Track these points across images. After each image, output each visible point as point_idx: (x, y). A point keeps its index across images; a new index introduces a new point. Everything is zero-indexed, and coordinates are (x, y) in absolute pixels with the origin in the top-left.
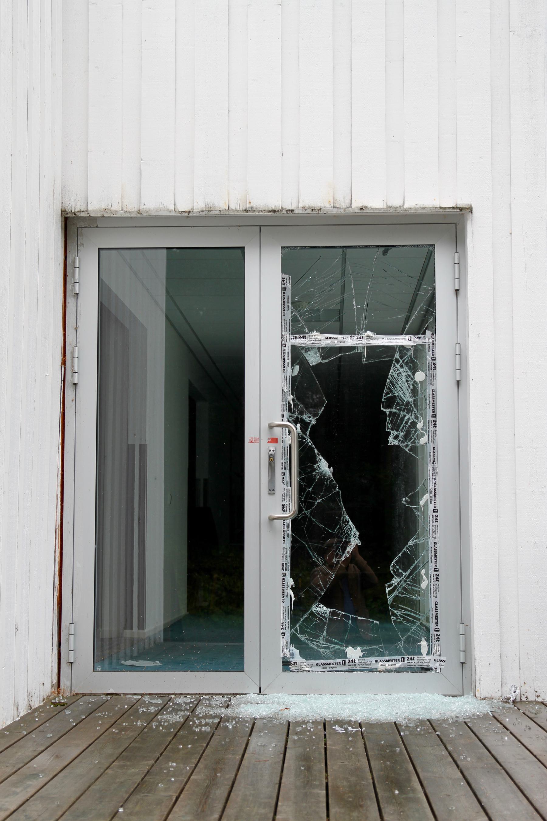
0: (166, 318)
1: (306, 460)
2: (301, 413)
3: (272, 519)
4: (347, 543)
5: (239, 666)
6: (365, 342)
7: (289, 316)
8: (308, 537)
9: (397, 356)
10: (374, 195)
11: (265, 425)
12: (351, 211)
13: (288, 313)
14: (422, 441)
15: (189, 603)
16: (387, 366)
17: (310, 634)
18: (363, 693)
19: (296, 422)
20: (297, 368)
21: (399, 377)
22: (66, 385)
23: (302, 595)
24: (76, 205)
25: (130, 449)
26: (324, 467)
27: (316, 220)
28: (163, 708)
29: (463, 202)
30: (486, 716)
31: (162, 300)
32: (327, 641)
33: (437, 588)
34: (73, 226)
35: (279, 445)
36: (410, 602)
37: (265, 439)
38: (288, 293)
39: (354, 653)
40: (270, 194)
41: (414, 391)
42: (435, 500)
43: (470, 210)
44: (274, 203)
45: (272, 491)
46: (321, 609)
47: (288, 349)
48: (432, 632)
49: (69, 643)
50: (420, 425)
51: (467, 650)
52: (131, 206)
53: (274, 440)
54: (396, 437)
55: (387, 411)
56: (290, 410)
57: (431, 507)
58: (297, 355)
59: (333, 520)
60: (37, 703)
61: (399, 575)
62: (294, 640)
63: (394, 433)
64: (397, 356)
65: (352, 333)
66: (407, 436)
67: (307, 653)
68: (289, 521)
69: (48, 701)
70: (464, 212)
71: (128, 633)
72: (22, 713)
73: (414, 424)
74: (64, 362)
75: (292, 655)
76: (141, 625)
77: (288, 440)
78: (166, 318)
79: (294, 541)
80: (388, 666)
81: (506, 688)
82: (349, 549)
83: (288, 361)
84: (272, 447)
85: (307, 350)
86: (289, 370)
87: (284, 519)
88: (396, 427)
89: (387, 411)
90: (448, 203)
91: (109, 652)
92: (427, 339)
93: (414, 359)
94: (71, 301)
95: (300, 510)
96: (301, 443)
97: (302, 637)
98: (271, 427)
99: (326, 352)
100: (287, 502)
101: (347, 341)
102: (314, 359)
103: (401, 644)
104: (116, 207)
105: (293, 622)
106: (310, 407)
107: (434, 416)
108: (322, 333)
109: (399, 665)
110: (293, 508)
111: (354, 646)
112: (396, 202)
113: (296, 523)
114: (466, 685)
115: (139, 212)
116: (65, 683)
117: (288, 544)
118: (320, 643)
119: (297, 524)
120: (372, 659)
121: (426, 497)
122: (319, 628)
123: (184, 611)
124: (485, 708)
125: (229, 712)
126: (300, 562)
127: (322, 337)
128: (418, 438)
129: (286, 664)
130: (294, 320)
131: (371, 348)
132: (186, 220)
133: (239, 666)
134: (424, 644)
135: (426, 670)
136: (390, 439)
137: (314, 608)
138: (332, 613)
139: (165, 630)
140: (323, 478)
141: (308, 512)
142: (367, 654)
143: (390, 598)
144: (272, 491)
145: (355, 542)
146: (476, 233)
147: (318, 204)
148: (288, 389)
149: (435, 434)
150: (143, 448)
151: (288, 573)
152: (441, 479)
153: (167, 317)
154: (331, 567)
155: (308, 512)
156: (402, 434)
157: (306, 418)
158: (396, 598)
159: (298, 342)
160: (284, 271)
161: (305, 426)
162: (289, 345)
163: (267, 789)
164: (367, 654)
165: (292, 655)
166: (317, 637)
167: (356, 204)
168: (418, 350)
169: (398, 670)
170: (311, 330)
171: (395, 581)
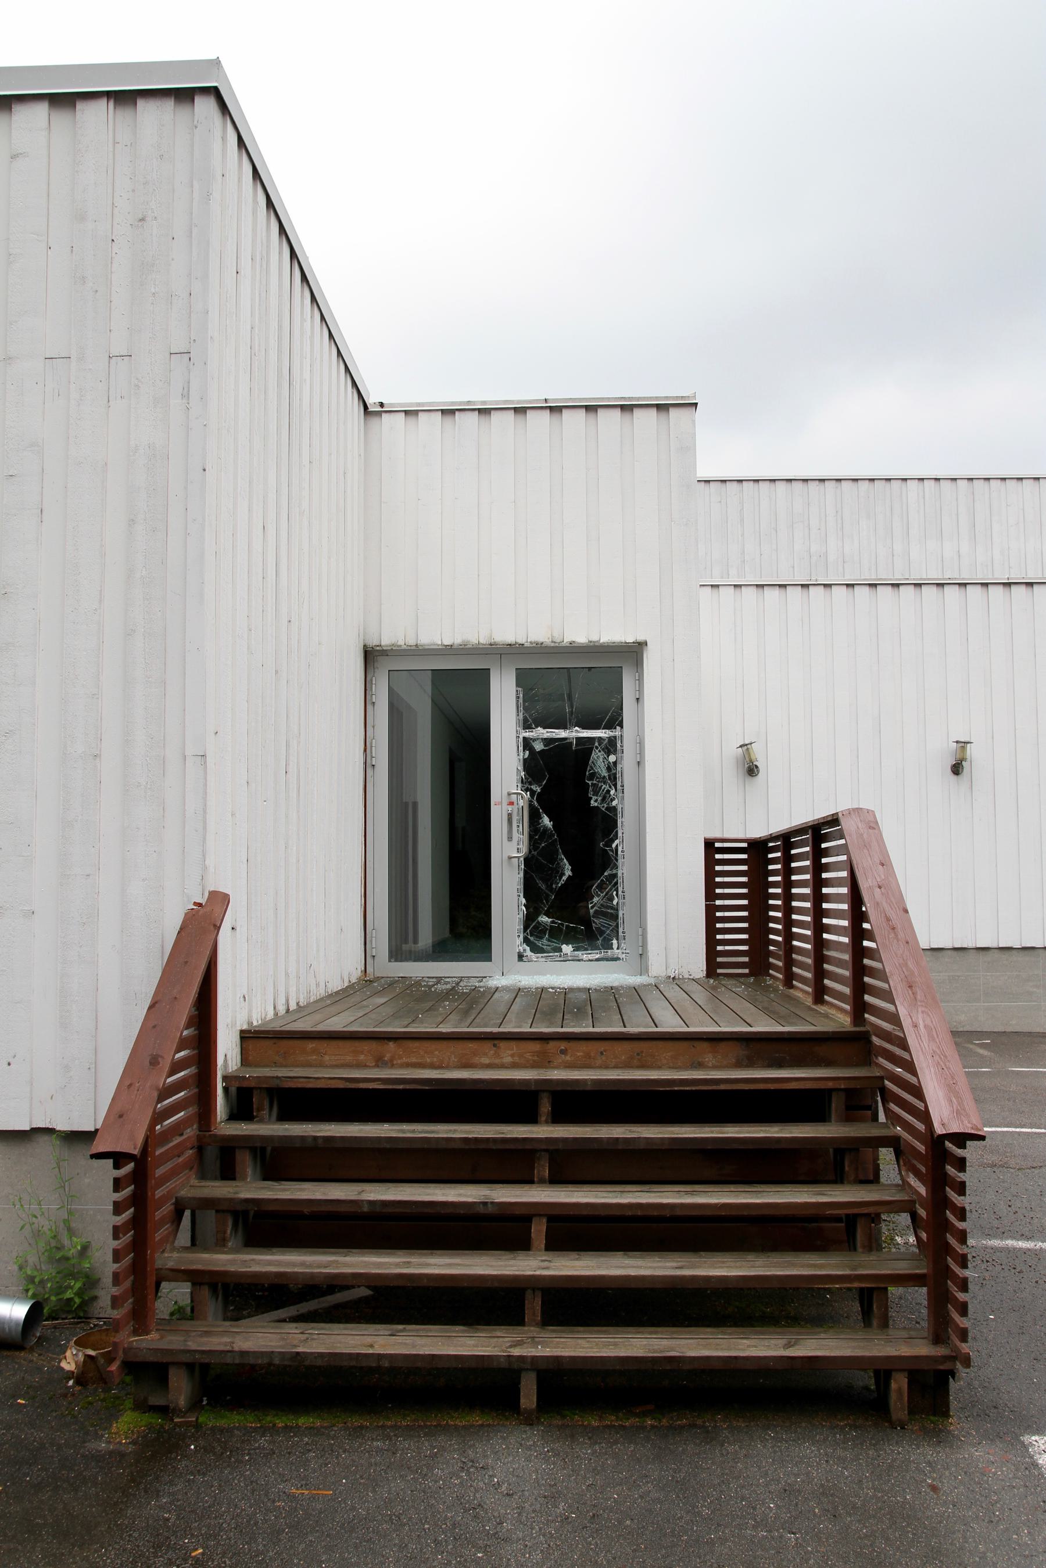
0: (436, 717)
1: (534, 817)
2: (530, 784)
3: (510, 858)
4: (563, 874)
5: (489, 958)
6: (574, 735)
7: (521, 717)
8: (536, 870)
9: (597, 744)
10: (579, 632)
11: (505, 793)
12: (563, 644)
13: (521, 714)
14: (614, 803)
15: (452, 930)
16: (590, 751)
17: (537, 937)
18: (572, 972)
19: (526, 790)
20: (527, 752)
21: (599, 760)
22: (368, 766)
23: (531, 910)
24: (372, 642)
25: (407, 804)
26: (546, 821)
27: (539, 650)
28: (438, 982)
29: (641, 638)
30: (651, 985)
31: (429, 688)
32: (549, 941)
33: (624, 903)
34: (371, 656)
35: (515, 807)
36: (612, 915)
37: (505, 802)
38: (521, 701)
39: (567, 949)
40: (507, 634)
41: (609, 769)
42: (624, 843)
43: (646, 643)
44: (510, 639)
45: (510, 839)
46: (544, 919)
47: (521, 740)
48: (620, 934)
49: (373, 943)
50: (612, 792)
51: (644, 945)
52: (412, 642)
53: (511, 803)
54: (596, 801)
55: (590, 783)
56: (522, 782)
57: (620, 849)
58: (527, 743)
59: (552, 858)
60: (354, 981)
61: (598, 896)
62: (526, 940)
63: (594, 798)
64: (597, 744)
65: (565, 728)
66: (604, 800)
67: (535, 949)
68: (522, 859)
69: (359, 979)
70: (641, 645)
71: (405, 947)
72: (346, 985)
73: (608, 792)
74: (365, 750)
75: (525, 950)
76: (416, 941)
77: (521, 803)
78: (436, 717)
79: (526, 873)
80: (590, 957)
81: (669, 970)
82: (564, 878)
83: (521, 748)
84: (510, 808)
85: (534, 740)
86: (522, 754)
87: (518, 858)
88: (596, 794)
89: (590, 783)
90: (630, 639)
91: (396, 954)
92: (617, 732)
93: (611, 746)
94: (369, 707)
95: (530, 851)
96: (531, 806)
97: (532, 939)
98: (509, 794)
99: (547, 741)
100: (521, 846)
101: (562, 734)
102: (539, 747)
103: (599, 942)
104: (401, 643)
105: (525, 929)
106: (538, 782)
107: (623, 786)
108: (544, 728)
109: (597, 956)
110: (524, 849)
111: (567, 944)
112: (594, 638)
113: (527, 860)
114: (643, 970)
115: (416, 645)
116: (369, 969)
117: (522, 875)
118: (544, 942)
119: (528, 861)
120: (580, 953)
121: (617, 842)
122: (543, 932)
123: (447, 934)
124: (652, 981)
125: (481, 984)
126: (530, 890)
127: (545, 731)
128: (612, 800)
129: (520, 957)
130: (525, 720)
131: (578, 739)
132: (449, 651)
133: (489, 958)
134: (615, 942)
135: (617, 959)
136: (592, 802)
137: (540, 919)
138: (553, 922)
139: (433, 946)
140: (546, 829)
141: (535, 853)
142: (576, 949)
143: (592, 911)
144: (510, 839)
145: (568, 872)
146: (651, 660)
147: (541, 639)
148: (521, 768)
149: (623, 798)
150: (415, 804)
151: (522, 895)
152: (626, 829)
153: (433, 700)
154: (551, 890)
155: (535, 853)
156: (600, 799)
157: (533, 787)
158: (596, 912)
159: (527, 734)
160: (517, 685)
161: (533, 793)
162: (521, 737)
163: (502, 1009)
164: (576, 949)
165: (525, 950)
166: (542, 938)
167: (567, 639)
168: (612, 741)
169: (597, 960)
170: (537, 727)
171: (596, 900)
